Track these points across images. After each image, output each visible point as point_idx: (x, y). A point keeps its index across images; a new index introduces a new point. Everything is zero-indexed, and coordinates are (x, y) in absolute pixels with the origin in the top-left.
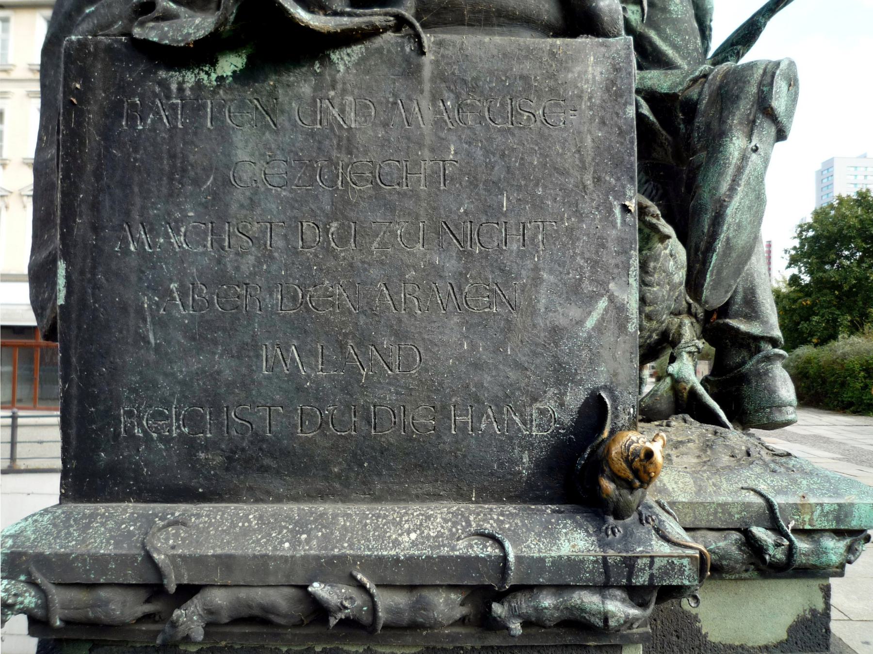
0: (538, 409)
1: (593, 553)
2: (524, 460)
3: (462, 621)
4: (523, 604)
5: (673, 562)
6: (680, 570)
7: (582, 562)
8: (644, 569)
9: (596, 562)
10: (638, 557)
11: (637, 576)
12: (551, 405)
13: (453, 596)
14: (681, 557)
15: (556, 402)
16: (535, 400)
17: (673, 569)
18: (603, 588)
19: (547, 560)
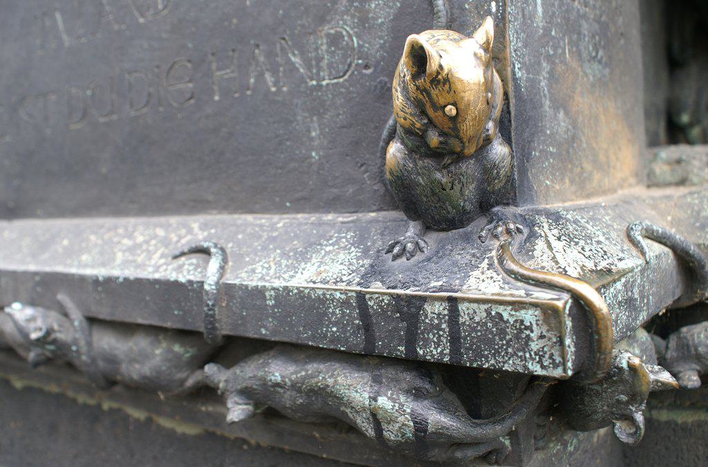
0: (328, 35)
1: (342, 286)
2: (313, 134)
3: (680, 372)
4: (249, 371)
5: (500, 316)
6: (517, 337)
7: (322, 301)
8: (438, 326)
9: (345, 303)
10: (423, 299)
11: (427, 342)
12: (345, 26)
13: (177, 348)
14: (518, 305)
15: (353, 16)
16: (322, 20)
17: (502, 333)
18: (362, 357)
19: (267, 294)
